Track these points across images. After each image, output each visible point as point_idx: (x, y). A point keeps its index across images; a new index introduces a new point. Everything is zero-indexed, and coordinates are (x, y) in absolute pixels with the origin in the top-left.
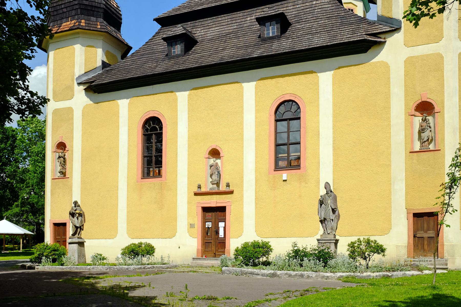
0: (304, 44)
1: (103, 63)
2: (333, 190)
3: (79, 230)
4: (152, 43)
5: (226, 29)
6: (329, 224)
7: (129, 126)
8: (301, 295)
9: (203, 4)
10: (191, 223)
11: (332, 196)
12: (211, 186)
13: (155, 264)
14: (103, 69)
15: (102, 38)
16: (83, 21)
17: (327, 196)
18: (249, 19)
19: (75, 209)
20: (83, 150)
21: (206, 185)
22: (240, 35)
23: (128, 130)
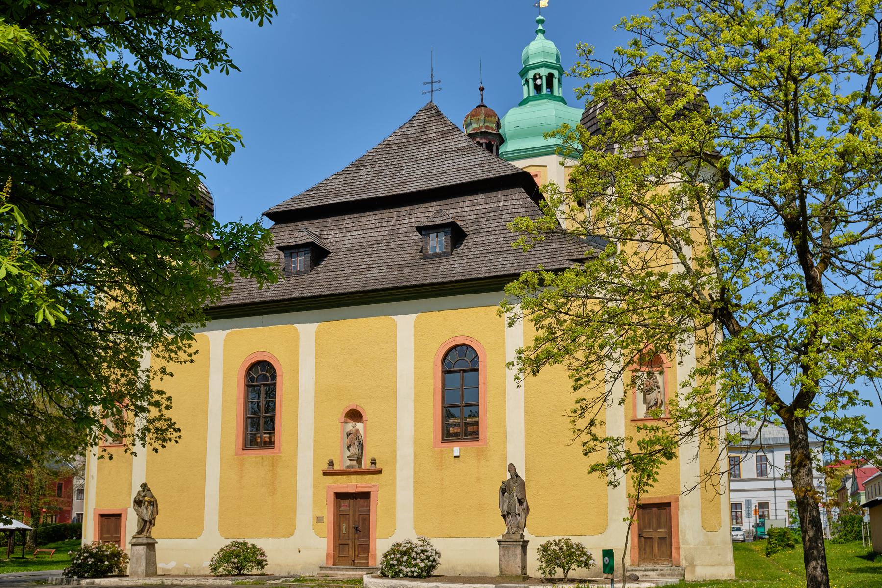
0: (483, 268)
2: (527, 470)
3: (148, 524)
5: (372, 234)
7: (224, 373)
9: (338, 194)
10: (318, 516)
11: (519, 482)
12: (349, 463)
17: (511, 483)
18: (406, 221)
19: (143, 494)
22: (393, 247)
23: (224, 378)
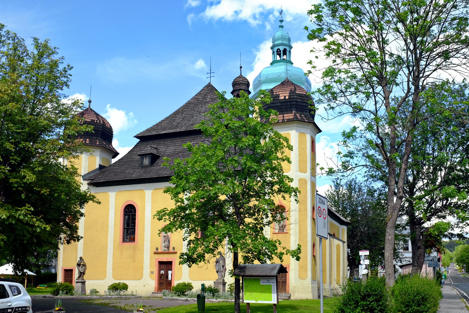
1: (100, 165)
3: (82, 274)
4: (132, 153)
5: (178, 148)
12: (164, 249)
13: (128, 295)
14: (100, 170)
15: (100, 150)
16: (88, 140)
17: (220, 259)
19: (80, 261)
20: (114, 263)
21: (161, 248)
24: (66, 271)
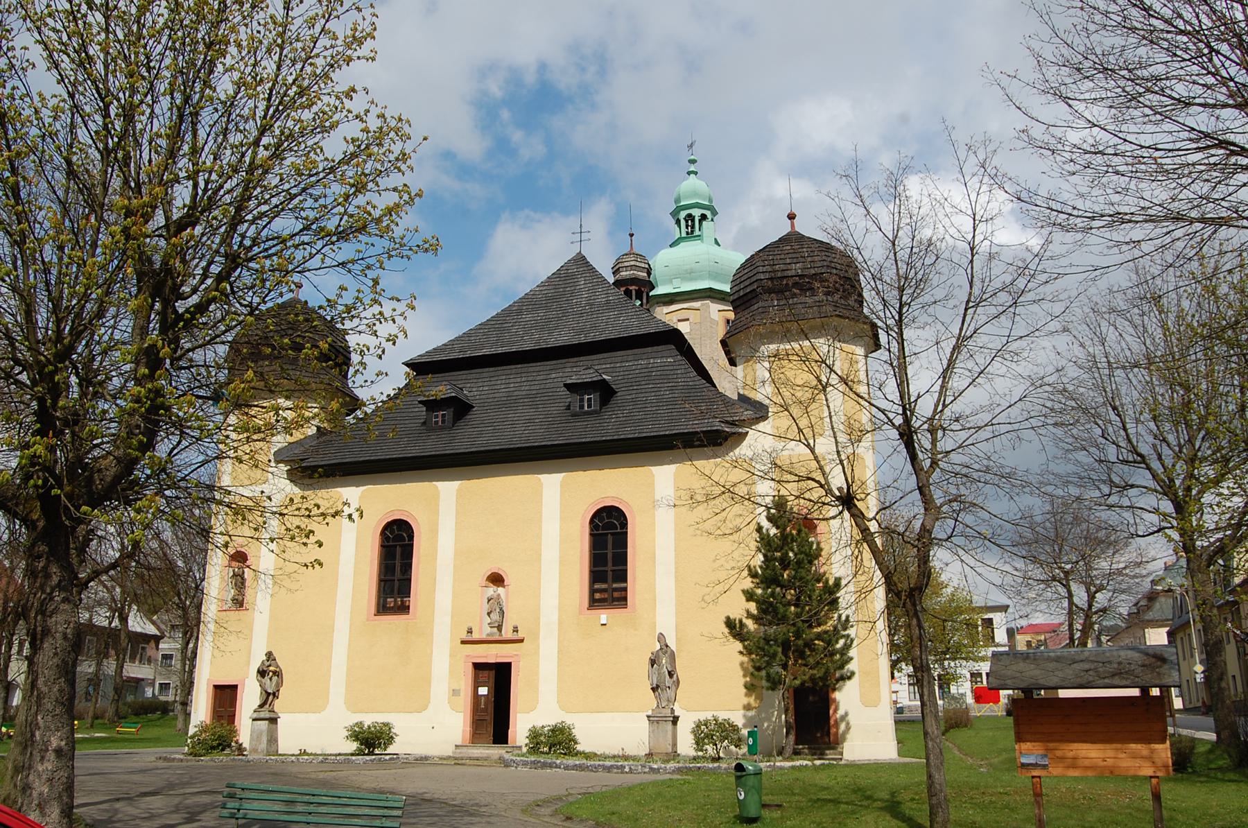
3: (271, 697)
6: (664, 696)
8: (1058, 371)
12: (489, 630)
17: (660, 653)
21: (481, 628)
24: (219, 689)
